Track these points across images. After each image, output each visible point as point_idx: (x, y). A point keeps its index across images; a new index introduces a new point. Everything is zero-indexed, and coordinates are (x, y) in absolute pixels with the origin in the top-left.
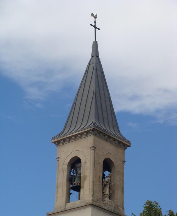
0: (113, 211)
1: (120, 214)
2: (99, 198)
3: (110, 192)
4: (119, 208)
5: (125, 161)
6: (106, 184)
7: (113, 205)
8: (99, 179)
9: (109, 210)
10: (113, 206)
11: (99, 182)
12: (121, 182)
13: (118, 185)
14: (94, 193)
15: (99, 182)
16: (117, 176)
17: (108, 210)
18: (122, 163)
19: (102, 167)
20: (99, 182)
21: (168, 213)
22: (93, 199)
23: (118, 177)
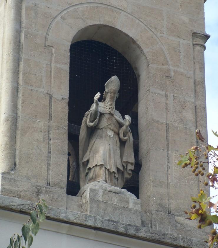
0: (121, 229)
1: (168, 241)
2: (48, 184)
3: (124, 160)
4: (177, 218)
5: (208, 32)
6: (126, 138)
7: (131, 206)
8: (50, 108)
9: (99, 225)
10: (130, 210)
11: (50, 116)
12: (189, 115)
13: (167, 125)
14: (15, 164)
15: (50, 116)
16: (163, 93)
17: (90, 223)
18: (186, 42)
19: (68, 60)
20: (50, 119)
21: (48, 79)
22: (7, 187)
23: (166, 96)
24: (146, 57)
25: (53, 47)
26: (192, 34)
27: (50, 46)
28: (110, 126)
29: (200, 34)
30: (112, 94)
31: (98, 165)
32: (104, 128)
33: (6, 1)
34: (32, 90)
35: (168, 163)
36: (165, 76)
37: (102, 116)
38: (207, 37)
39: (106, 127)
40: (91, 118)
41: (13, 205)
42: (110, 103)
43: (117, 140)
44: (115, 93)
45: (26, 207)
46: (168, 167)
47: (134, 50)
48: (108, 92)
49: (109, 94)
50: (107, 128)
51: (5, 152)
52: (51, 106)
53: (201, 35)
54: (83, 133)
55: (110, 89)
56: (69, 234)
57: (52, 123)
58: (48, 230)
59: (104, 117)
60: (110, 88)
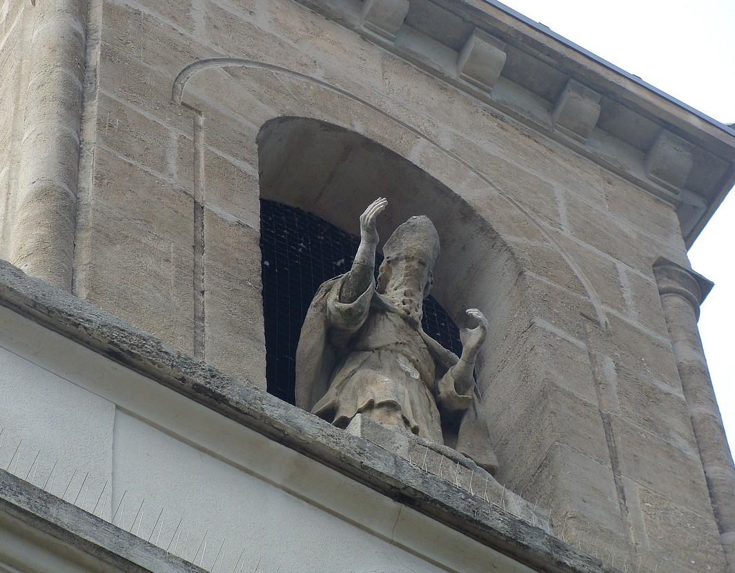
16: (582, 344)
24: (513, 254)
25: (200, 113)
26: (654, 266)
27: (192, 108)
28: (407, 349)
29: (679, 267)
30: (414, 264)
31: (377, 402)
32: (386, 348)
33: (34, 3)
34: (131, 165)
35: (622, 501)
36: (582, 314)
37: (379, 315)
38: (702, 287)
39: (393, 347)
40: (344, 289)
41: (83, 319)
42: (405, 289)
43: (430, 397)
44: (421, 263)
45: (135, 340)
46: (624, 508)
47: (464, 248)
48: (397, 259)
49: (403, 264)
50: (397, 351)
51: (41, 231)
52: (198, 224)
53: (684, 271)
54: (310, 339)
55: (407, 249)
56: (293, 489)
57: (204, 259)
58: (214, 455)
59: (386, 320)
60: (405, 246)
